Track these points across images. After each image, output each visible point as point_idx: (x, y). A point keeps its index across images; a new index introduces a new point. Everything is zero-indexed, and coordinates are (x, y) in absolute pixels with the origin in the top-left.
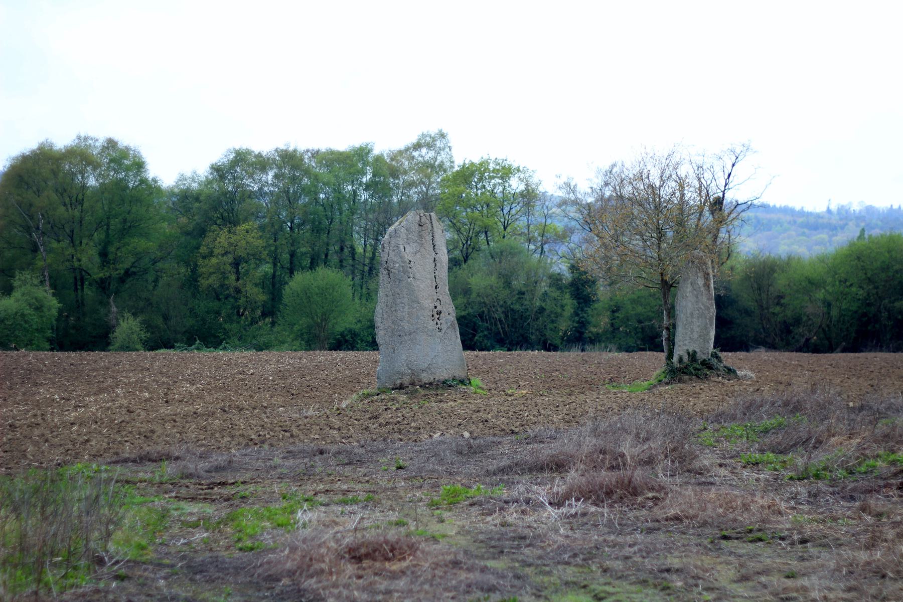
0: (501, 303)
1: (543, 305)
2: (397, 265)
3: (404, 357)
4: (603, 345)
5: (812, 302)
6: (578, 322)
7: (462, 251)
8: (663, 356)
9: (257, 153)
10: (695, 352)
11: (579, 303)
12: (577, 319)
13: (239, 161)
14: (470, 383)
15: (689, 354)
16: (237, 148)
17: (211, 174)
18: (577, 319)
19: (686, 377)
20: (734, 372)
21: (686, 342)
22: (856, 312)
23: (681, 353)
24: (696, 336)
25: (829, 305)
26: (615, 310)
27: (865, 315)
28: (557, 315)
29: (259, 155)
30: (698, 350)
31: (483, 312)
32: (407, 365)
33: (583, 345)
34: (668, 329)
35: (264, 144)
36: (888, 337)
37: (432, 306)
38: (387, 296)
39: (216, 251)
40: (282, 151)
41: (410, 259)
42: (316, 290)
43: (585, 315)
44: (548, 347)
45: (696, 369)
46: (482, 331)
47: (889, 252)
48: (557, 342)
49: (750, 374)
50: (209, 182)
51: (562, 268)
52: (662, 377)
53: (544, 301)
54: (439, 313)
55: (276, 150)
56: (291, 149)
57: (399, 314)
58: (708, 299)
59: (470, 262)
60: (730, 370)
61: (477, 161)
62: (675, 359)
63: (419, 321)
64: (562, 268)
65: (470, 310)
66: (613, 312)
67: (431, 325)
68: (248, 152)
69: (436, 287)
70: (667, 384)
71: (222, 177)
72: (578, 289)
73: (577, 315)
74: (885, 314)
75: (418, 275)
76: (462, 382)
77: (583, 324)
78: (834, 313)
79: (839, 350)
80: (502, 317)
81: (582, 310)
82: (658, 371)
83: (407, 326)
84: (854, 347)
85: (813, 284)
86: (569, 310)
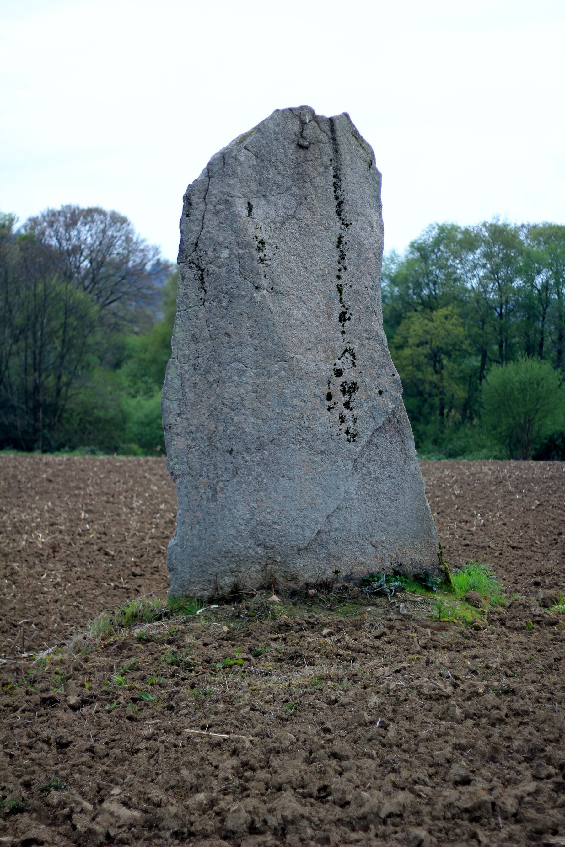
2: (225, 254)
3: (242, 510)
9: (463, 229)
13: (443, 239)
14: (447, 581)
16: (441, 223)
17: (412, 252)
29: (467, 232)
32: (252, 534)
35: (470, 216)
37: (327, 369)
38: (195, 339)
39: (411, 341)
40: (491, 225)
41: (265, 236)
42: (517, 385)
50: (410, 264)
54: (350, 389)
55: (484, 225)
56: (500, 223)
57: (229, 391)
63: (287, 411)
67: (325, 421)
68: (454, 228)
69: (342, 318)
71: (424, 257)
75: (284, 283)
76: (422, 580)
83: (250, 425)
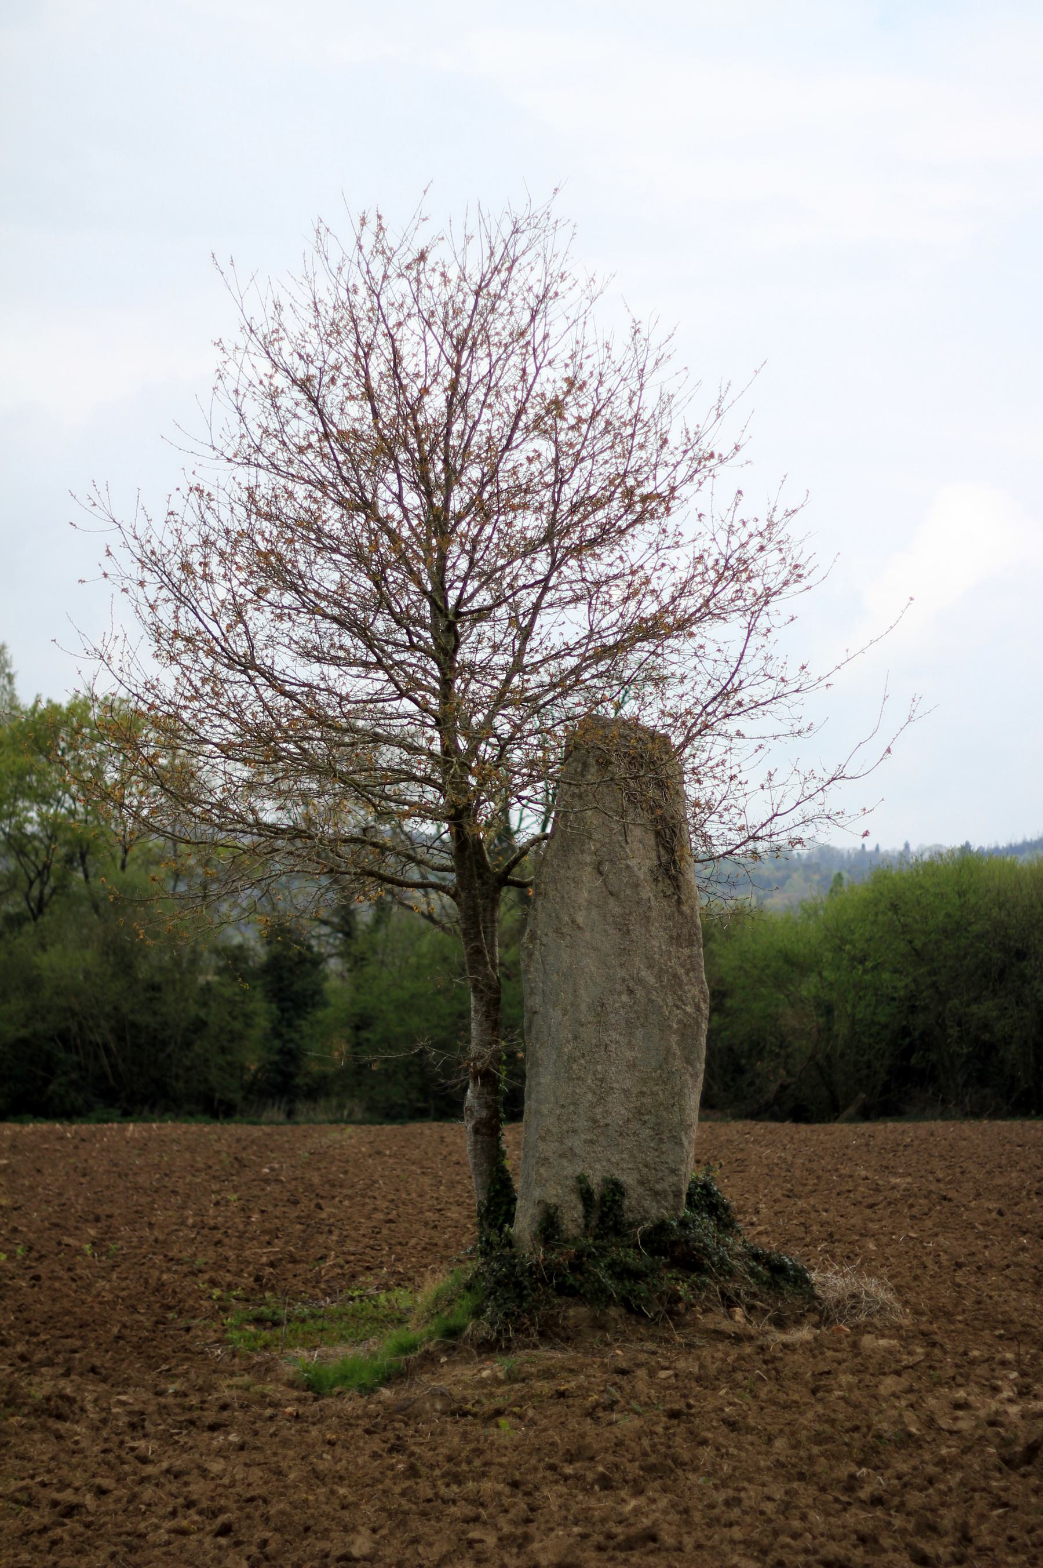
0: (108, 1009)
1: (202, 1013)
4: (334, 1101)
5: (792, 1005)
6: (280, 1052)
7: (27, 897)
8: (459, 1137)
10: (616, 1188)
11: (283, 1010)
12: (277, 1043)
15: (586, 1195)
18: (277, 1043)
19: (576, 1313)
20: (800, 1280)
21: (576, 1142)
22: (886, 1026)
23: (553, 1194)
24: (618, 1111)
25: (828, 1010)
26: (361, 1023)
27: (905, 1032)
28: (236, 1037)
30: (628, 1179)
31: (68, 1029)
33: (291, 1101)
34: (487, 1078)
36: (960, 1080)
43: (296, 1036)
44: (217, 1108)
45: (623, 1272)
46: (65, 1073)
47: (961, 894)
48: (237, 1097)
49: (876, 1289)
51: (248, 936)
52: (460, 1313)
53: (205, 1004)
58: (675, 940)
59: (45, 919)
60: (778, 1269)
61: (64, 700)
62: (524, 1224)
64: (248, 936)
65: (40, 1026)
66: (358, 1028)
70: (488, 1347)
72: (281, 979)
73: (278, 1035)
74: (954, 1032)
77: (291, 1056)
78: (842, 1028)
79: (851, 1110)
80: (110, 1038)
81: (290, 1025)
82: (436, 1283)
84: (883, 1107)
85: (793, 964)
86: (263, 1023)
